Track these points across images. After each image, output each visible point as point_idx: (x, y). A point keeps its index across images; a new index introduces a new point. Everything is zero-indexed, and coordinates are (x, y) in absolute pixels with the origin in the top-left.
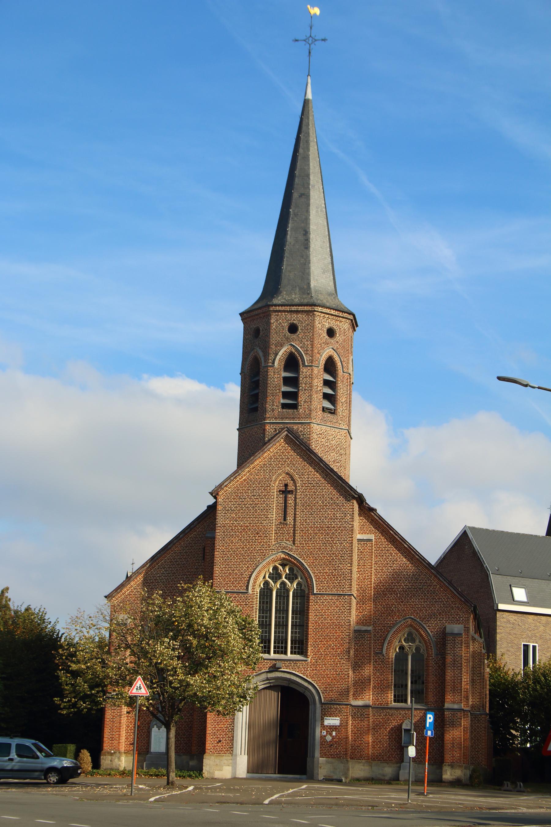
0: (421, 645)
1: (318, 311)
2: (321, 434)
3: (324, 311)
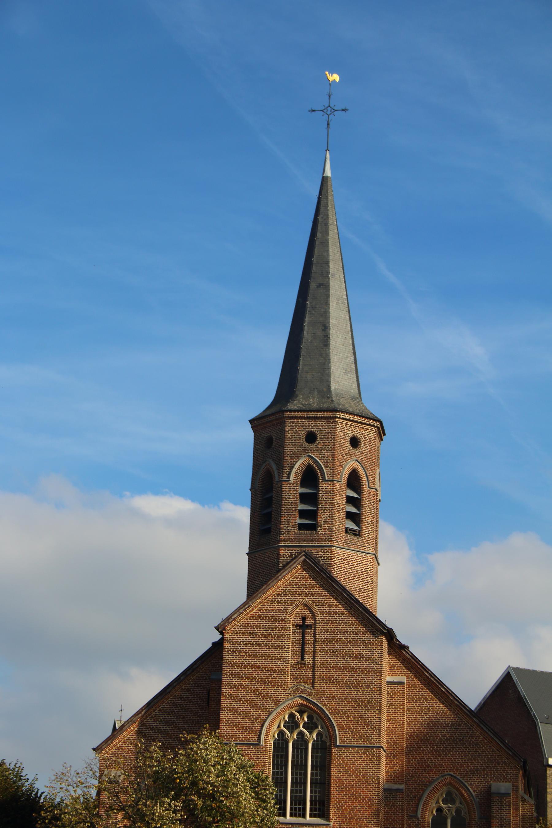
0: (462, 806)
1: (339, 418)
2: (344, 559)
3: (346, 417)
